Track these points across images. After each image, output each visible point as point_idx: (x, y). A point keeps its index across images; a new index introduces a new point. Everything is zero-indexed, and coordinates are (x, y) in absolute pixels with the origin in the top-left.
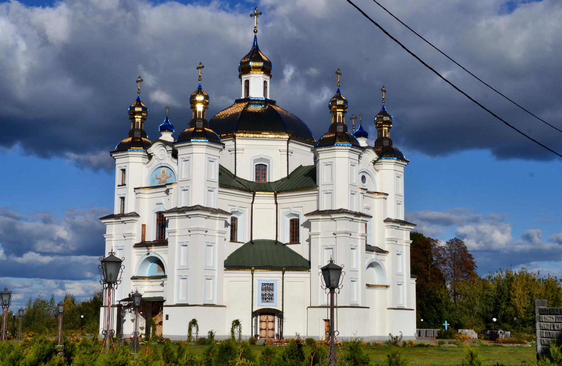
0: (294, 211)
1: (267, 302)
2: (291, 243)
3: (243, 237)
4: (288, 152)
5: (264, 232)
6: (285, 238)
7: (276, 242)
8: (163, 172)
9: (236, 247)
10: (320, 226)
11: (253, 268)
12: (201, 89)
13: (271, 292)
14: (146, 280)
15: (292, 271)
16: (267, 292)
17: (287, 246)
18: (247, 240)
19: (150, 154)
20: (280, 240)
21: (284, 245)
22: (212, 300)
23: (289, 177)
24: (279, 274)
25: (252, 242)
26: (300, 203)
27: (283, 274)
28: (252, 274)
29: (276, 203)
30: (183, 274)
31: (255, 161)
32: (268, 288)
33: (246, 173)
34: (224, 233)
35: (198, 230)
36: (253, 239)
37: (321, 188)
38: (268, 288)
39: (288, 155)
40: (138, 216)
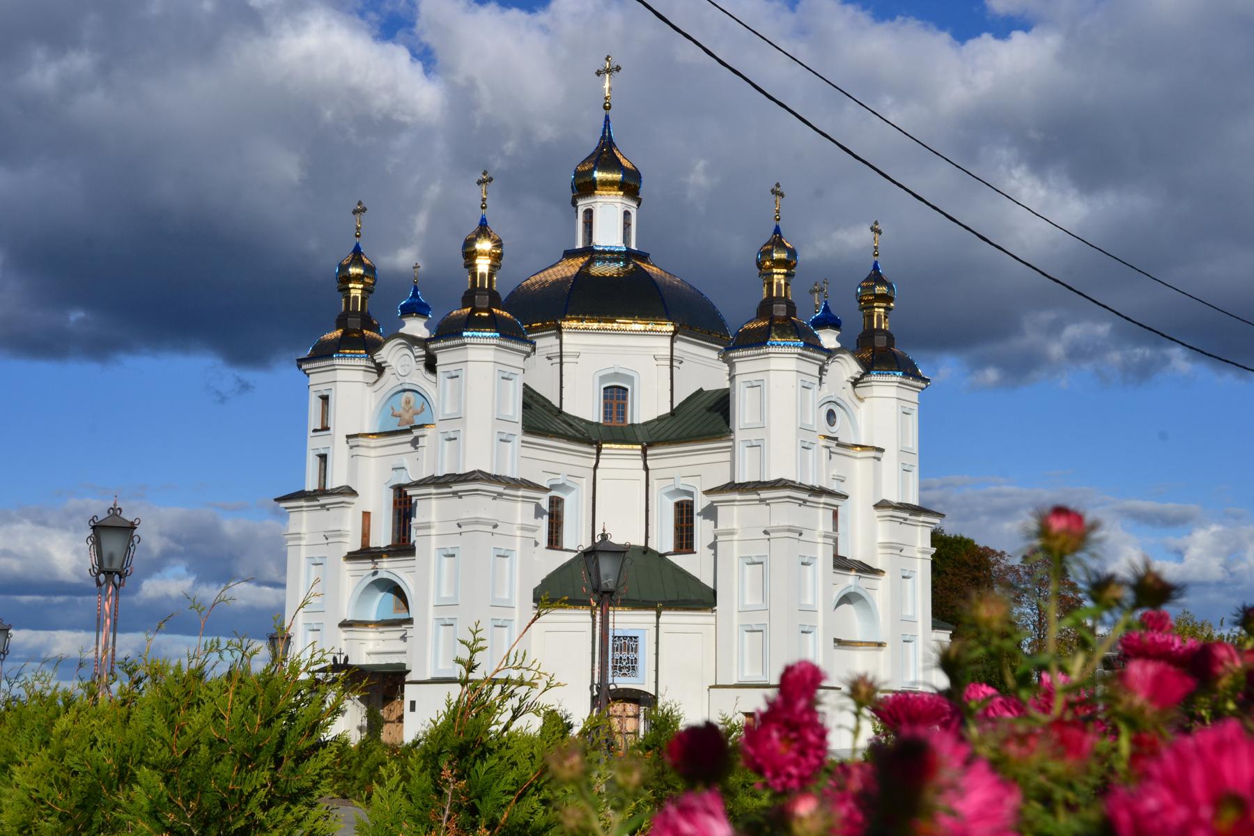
0: (682, 484)
3: (576, 537)
4: (672, 360)
6: (663, 541)
7: (646, 550)
8: (408, 402)
10: (735, 514)
13: (632, 655)
15: (676, 609)
16: (625, 655)
19: (380, 364)
20: (653, 545)
21: (663, 556)
23: (673, 413)
24: (648, 617)
26: (694, 468)
27: (658, 617)
29: (646, 469)
31: (603, 379)
33: (584, 405)
37: (739, 435)
39: (672, 366)
40: (354, 493)
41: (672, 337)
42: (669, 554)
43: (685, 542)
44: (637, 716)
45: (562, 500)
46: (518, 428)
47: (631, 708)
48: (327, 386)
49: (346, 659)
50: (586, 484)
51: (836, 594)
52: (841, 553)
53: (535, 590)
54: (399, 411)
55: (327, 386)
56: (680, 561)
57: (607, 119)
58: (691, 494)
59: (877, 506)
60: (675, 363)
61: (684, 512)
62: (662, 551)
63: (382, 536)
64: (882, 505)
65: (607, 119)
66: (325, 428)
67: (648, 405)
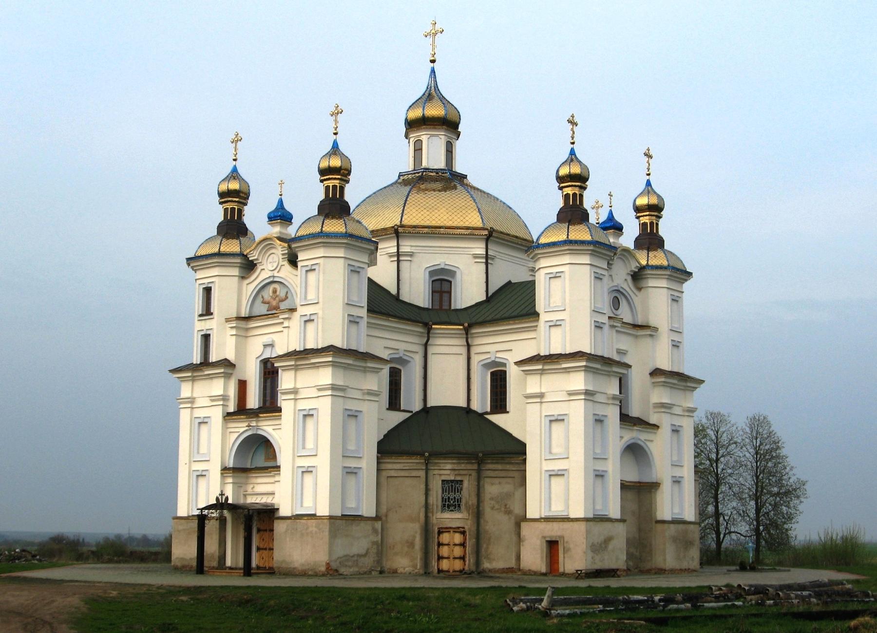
3: (412, 401)
6: (481, 402)
7: (468, 411)
8: (275, 291)
9: (397, 418)
11: (427, 454)
12: (338, 147)
18: (417, 406)
19: (252, 261)
20: (476, 406)
21: (481, 415)
23: (489, 299)
26: (508, 346)
33: (417, 293)
36: (429, 405)
37: (543, 317)
42: (487, 413)
43: (499, 403)
45: (400, 370)
46: (363, 312)
50: (418, 359)
52: (489, 410)
53: (380, 443)
56: (496, 419)
57: (433, 71)
60: (489, 261)
62: (480, 411)
63: (253, 401)
64: (656, 372)
65: (433, 71)
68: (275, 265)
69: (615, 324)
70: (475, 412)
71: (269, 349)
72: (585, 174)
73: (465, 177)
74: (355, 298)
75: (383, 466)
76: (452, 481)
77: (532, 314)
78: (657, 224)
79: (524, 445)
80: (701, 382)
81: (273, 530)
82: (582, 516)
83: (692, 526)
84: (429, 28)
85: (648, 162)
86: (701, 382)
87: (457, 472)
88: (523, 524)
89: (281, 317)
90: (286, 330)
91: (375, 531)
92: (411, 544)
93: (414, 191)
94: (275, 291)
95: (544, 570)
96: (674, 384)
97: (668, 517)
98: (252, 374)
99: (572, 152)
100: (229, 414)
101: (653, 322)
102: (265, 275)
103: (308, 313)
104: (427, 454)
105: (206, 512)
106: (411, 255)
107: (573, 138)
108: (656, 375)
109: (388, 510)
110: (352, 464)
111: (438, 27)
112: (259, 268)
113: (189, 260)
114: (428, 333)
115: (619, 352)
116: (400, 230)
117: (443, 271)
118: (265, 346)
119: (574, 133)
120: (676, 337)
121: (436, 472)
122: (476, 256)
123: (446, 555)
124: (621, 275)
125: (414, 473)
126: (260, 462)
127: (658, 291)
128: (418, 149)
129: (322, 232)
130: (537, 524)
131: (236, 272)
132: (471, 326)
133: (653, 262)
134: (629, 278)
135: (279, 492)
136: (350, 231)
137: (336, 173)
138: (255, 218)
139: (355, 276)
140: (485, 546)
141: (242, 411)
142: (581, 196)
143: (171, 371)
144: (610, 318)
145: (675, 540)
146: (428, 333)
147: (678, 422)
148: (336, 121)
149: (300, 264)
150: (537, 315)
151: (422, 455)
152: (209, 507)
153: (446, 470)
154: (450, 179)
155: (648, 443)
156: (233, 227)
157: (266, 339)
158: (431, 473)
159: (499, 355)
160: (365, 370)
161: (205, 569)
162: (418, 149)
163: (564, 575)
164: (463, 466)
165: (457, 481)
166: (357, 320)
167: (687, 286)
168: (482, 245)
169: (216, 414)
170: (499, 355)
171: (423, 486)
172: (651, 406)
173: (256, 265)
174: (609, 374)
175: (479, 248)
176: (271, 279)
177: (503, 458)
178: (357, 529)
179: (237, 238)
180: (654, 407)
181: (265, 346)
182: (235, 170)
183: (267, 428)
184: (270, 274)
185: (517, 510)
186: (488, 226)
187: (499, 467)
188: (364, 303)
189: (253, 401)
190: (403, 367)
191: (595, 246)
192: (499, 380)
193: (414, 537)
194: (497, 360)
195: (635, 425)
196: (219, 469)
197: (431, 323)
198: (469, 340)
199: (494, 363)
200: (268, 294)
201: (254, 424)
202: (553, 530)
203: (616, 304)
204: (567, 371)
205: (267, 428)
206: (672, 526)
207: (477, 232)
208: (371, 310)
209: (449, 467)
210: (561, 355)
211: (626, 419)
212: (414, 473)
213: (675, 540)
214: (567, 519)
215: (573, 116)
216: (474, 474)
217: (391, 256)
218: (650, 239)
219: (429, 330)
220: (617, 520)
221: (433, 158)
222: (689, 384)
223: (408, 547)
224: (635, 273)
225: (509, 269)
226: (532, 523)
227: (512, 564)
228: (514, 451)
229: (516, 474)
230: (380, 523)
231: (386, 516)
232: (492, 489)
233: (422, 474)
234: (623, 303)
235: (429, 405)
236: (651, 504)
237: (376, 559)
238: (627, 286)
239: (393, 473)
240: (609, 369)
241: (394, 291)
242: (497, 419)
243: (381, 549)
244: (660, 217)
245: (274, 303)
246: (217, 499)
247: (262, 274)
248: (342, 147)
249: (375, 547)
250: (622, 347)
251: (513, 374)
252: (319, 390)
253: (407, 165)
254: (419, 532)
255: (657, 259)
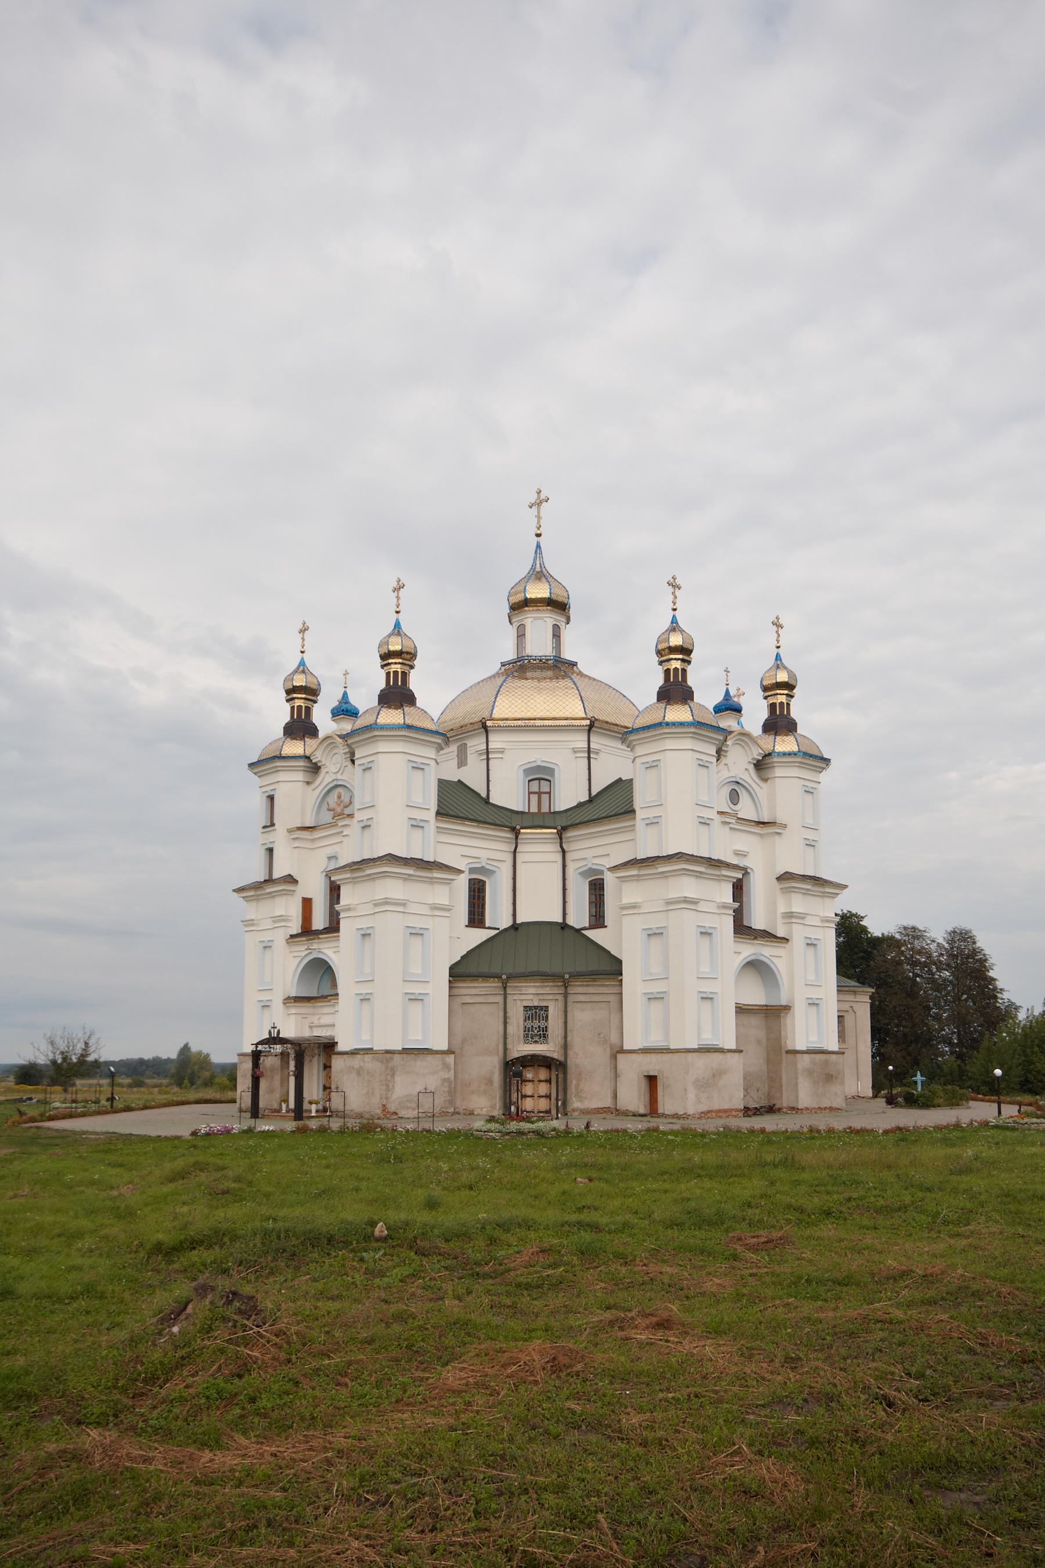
1: (536, 1042)
2: (592, 927)
3: (498, 916)
4: (589, 752)
5: (540, 905)
6: (579, 917)
7: (564, 926)
8: (339, 797)
9: (479, 936)
11: (504, 977)
12: (400, 628)
14: (501, 1028)
16: (536, 1024)
17: (583, 932)
18: (505, 923)
19: (316, 764)
20: (571, 921)
21: (578, 931)
22: (366, 1037)
23: (591, 800)
25: (515, 927)
26: (600, 849)
28: (566, 995)
29: (564, 852)
30: (364, 989)
31: (527, 772)
32: (536, 1013)
33: (509, 793)
34: (449, 910)
35: (387, 903)
36: (518, 921)
37: (640, 814)
38: (536, 1013)
39: (589, 758)
41: (589, 731)
42: (585, 929)
43: (598, 920)
44: (549, 1081)
45: (484, 882)
46: (431, 815)
47: (543, 1074)
48: (272, 787)
49: (279, 1032)
50: (506, 870)
51: (739, 960)
52: (587, 925)
53: (451, 968)
54: (332, 805)
55: (272, 787)
56: (593, 934)
57: (538, 546)
58: (602, 872)
59: (780, 878)
60: (592, 755)
61: (597, 888)
62: (577, 927)
63: (319, 921)
64: (785, 877)
65: (538, 546)
66: (273, 825)
67: (569, 793)
68: (338, 766)
69: (727, 820)
70: (572, 928)
71: (333, 861)
72: (792, 682)
73: (575, 664)
74: (418, 800)
75: (455, 991)
76: (536, 1007)
77: (630, 812)
78: (788, 704)
79: (620, 962)
80: (846, 886)
81: (330, 1067)
82: (734, 1047)
83: (834, 1056)
84: (533, 498)
85: (777, 632)
86: (846, 886)
87: (541, 997)
88: (619, 1056)
89: (340, 824)
90: (345, 839)
91: (446, 1066)
92: (490, 1082)
93: (510, 679)
94: (339, 797)
95: (642, 1111)
96: (808, 890)
97: (800, 1046)
98: (315, 888)
99: (674, 620)
100: (292, 936)
101: (780, 818)
102: (328, 779)
103: (365, 818)
104: (504, 977)
105: (260, 1048)
106: (502, 751)
107: (778, 641)
108: (784, 879)
109: (464, 1041)
110: (417, 989)
111: (543, 496)
112: (323, 771)
113: (251, 765)
114: (517, 838)
115: (737, 853)
116: (489, 723)
117: (539, 769)
118: (330, 858)
119: (676, 597)
120: (811, 835)
121: (516, 997)
122: (575, 751)
123: (529, 1093)
124: (739, 763)
125: (492, 999)
126: (327, 992)
127: (787, 780)
128: (521, 635)
129: (376, 723)
130: (634, 1056)
131: (300, 776)
132: (564, 829)
133: (779, 748)
134: (751, 767)
135: (346, 1025)
136: (409, 721)
137: (398, 658)
138: (321, 716)
139: (418, 774)
140: (574, 1082)
141: (307, 931)
142: (684, 671)
143: (236, 891)
144: (720, 813)
145: (810, 1072)
146: (517, 838)
147: (813, 934)
148: (398, 598)
149: (356, 762)
150: (633, 811)
151: (498, 977)
152: (261, 1043)
153: (529, 993)
154: (559, 668)
155: (774, 960)
156: (300, 727)
157: (329, 851)
158: (510, 999)
159: (596, 861)
160: (432, 881)
161: (261, 1112)
162: (521, 635)
163: (664, 1116)
164: (547, 990)
165: (541, 1008)
166: (421, 824)
167: (825, 777)
168: (584, 737)
169: (279, 937)
170: (596, 861)
171: (501, 1014)
172: (779, 916)
173: (320, 767)
174: (720, 879)
175: (580, 741)
176: (335, 783)
177: (595, 980)
178: (421, 1064)
179: (302, 738)
180: (783, 917)
181: (330, 858)
182: (302, 663)
183: (326, 950)
184: (334, 777)
185: (614, 1038)
186: (590, 715)
187: (591, 990)
188: (433, 807)
189: (319, 921)
190: (488, 878)
191: (696, 727)
192: (597, 888)
193: (493, 1073)
194: (594, 867)
195: (755, 938)
196: (340, 997)
197: (518, 827)
198: (564, 846)
199: (592, 871)
200: (332, 799)
201: (315, 946)
202: (652, 1064)
203: (734, 797)
204: (664, 875)
205: (326, 950)
206: (806, 1056)
207: (578, 723)
208: (441, 813)
209: (532, 991)
210: (658, 858)
211: (742, 929)
212: (492, 999)
213: (810, 1072)
214: (667, 1051)
215: (674, 578)
216: (560, 998)
217: (480, 754)
218: (779, 723)
219: (517, 834)
220: (730, 1051)
221: (539, 645)
222: (827, 890)
223: (486, 1084)
224: (758, 761)
225: (613, 763)
226: (629, 1055)
227: (608, 1103)
228: (609, 968)
229: (611, 998)
230: (452, 1056)
231: (462, 1049)
232: (582, 1016)
233: (500, 999)
234: (744, 796)
235: (518, 921)
236: (780, 1031)
237: (449, 1098)
238: (749, 777)
239: (468, 1000)
240: (718, 873)
241: (484, 795)
242: (595, 935)
243: (454, 1087)
244: (792, 697)
245: (339, 810)
246: (270, 1032)
247: (325, 779)
248: (405, 628)
249: (446, 1084)
250: (738, 847)
251: (609, 879)
252: (375, 905)
253: (510, 655)
254: (498, 1066)
255: (785, 744)
